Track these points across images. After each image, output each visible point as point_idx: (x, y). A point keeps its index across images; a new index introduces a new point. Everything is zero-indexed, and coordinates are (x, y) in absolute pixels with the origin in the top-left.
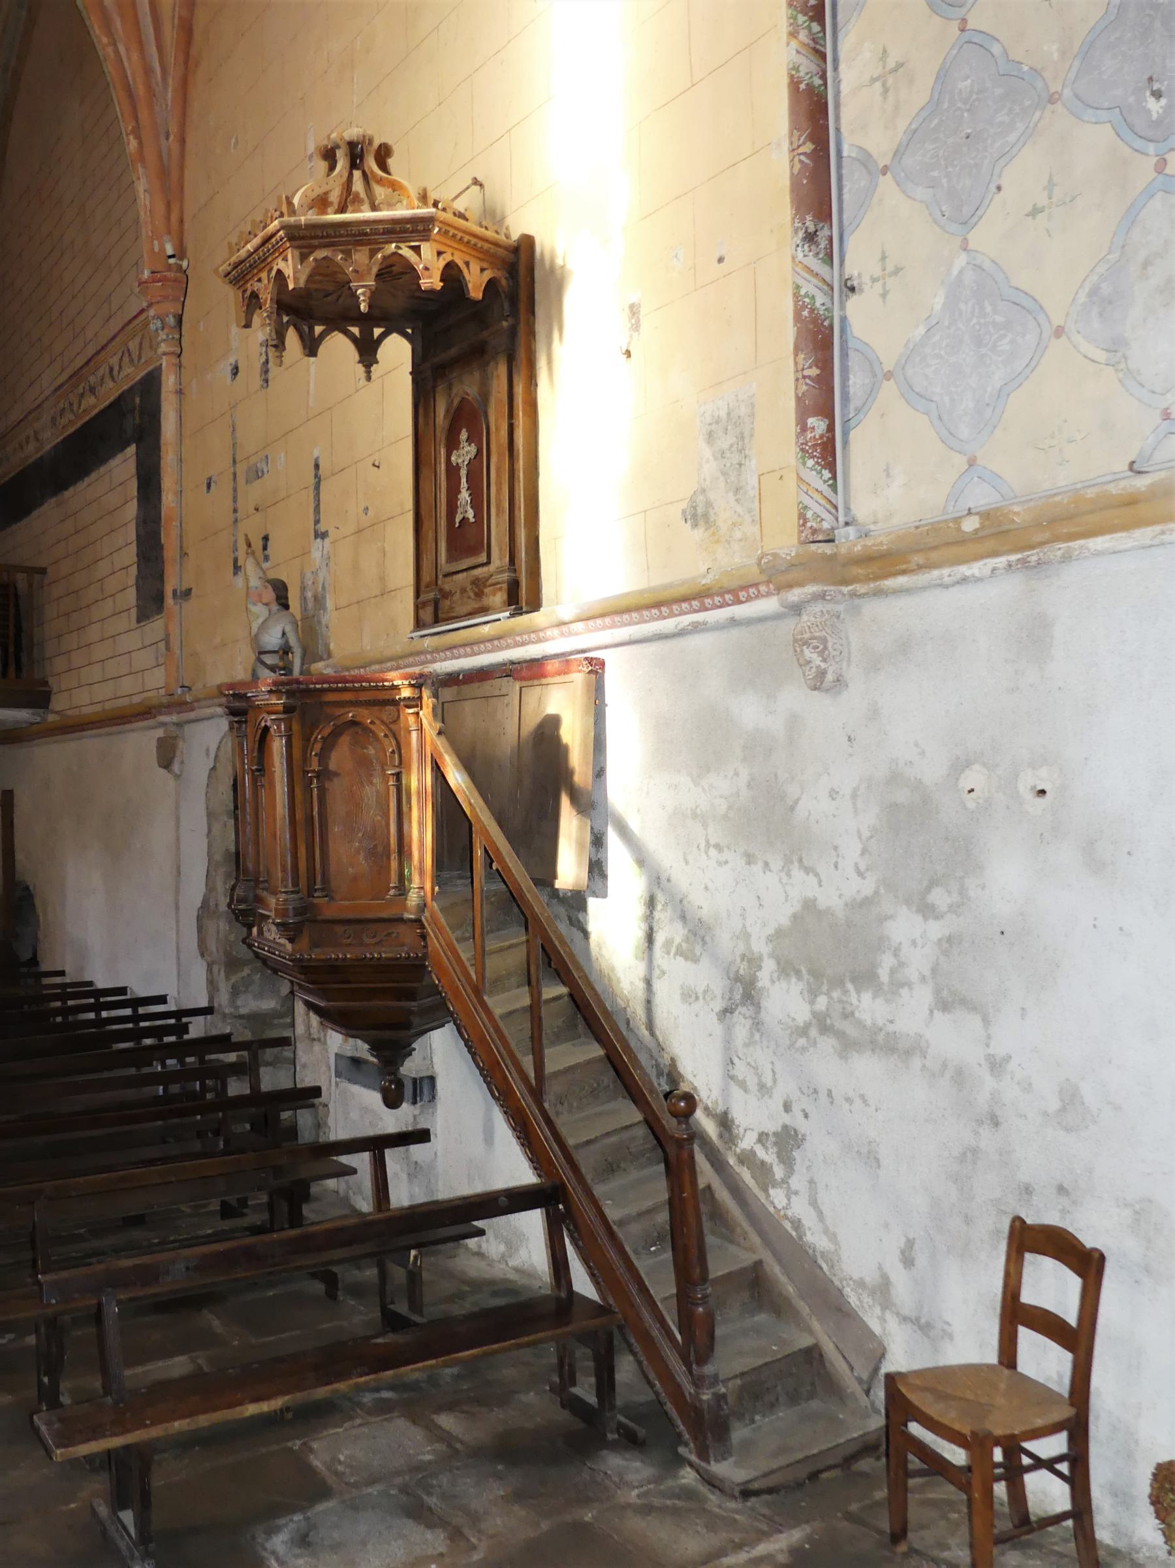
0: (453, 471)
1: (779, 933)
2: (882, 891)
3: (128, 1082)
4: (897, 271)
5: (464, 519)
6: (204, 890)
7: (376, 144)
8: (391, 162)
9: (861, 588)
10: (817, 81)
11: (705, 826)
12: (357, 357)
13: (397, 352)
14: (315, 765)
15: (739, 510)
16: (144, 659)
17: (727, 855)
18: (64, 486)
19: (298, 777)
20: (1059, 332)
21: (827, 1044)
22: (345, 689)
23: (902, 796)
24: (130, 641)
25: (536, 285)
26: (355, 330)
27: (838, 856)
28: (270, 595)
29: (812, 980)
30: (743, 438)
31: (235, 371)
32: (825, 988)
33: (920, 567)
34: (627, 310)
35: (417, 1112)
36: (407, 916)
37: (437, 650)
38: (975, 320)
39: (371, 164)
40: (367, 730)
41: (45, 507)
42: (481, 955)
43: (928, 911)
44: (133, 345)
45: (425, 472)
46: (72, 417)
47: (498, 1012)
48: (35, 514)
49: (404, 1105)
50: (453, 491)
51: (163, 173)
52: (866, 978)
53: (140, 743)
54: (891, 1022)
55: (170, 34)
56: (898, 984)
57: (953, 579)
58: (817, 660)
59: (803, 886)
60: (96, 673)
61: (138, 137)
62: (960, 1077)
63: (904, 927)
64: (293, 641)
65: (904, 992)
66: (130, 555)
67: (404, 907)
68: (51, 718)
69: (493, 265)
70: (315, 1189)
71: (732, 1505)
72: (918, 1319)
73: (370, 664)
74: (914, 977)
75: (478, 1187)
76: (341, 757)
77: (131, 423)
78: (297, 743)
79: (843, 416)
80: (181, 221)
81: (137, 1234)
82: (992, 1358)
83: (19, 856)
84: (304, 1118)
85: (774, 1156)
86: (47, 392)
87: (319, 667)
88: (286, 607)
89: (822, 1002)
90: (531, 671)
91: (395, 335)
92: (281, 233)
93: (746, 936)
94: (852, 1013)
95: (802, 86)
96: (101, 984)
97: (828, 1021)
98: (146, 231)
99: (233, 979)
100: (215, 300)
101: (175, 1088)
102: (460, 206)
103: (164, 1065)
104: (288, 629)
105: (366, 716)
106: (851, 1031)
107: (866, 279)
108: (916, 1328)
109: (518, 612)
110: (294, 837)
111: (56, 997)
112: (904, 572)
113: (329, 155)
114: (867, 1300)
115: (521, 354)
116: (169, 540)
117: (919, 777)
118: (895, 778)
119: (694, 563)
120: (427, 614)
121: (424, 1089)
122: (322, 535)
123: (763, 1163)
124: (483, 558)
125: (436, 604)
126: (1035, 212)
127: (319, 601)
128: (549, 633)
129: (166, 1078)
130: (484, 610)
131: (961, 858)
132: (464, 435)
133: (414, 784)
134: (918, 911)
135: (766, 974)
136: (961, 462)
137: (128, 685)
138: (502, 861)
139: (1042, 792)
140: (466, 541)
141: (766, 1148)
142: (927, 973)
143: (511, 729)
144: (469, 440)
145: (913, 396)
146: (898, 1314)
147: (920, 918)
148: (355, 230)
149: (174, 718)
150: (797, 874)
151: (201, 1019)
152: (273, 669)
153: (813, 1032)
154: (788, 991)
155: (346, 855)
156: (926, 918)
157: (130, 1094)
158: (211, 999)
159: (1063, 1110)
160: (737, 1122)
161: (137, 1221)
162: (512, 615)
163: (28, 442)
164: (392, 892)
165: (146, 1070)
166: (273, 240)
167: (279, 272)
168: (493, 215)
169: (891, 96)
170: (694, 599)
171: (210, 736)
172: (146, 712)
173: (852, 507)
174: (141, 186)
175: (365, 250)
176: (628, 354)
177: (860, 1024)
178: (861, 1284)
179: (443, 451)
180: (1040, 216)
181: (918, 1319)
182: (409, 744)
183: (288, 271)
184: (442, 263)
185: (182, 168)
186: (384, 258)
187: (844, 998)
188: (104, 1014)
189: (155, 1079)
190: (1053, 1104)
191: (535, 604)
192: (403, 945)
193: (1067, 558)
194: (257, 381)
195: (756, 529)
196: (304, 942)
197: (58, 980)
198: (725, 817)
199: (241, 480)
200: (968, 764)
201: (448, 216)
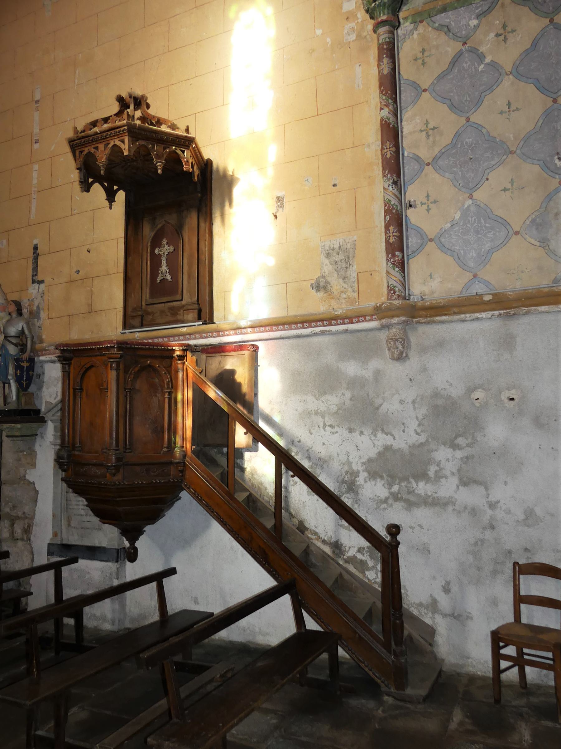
1: (370, 461)
2: (430, 440)
4: (435, 202)
5: (164, 280)
9: (422, 320)
10: (396, 126)
11: (323, 417)
12: (106, 198)
15: (346, 286)
17: (336, 429)
20: (517, 233)
21: (399, 505)
23: (440, 402)
27: (405, 427)
29: (389, 479)
30: (349, 257)
32: (397, 482)
33: (455, 313)
34: (275, 199)
35: (118, 566)
38: (476, 224)
40: (155, 370)
43: (455, 447)
52: (422, 476)
54: (436, 493)
56: (439, 476)
57: (471, 318)
58: (400, 347)
59: (382, 440)
62: (474, 512)
63: (442, 454)
65: (443, 480)
71: (420, 706)
72: (453, 614)
74: (448, 473)
79: (407, 253)
82: (512, 620)
85: (368, 557)
89: (395, 488)
90: (219, 350)
92: (126, 127)
93: (349, 463)
94: (413, 491)
95: (391, 126)
97: (399, 496)
106: (412, 498)
107: (418, 203)
108: (452, 618)
112: (446, 315)
114: (423, 611)
117: (449, 394)
118: (436, 395)
119: (317, 305)
123: (361, 560)
126: (505, 190)
128: (226, 333)
131: (473, 424)
134: (450, 447)
135: (360, 480)
136: (469, 276)
139: (512, 399)
141: (363, 555)
142: (455, 471)
145: (443, 248)
146: (441, 614)
147: (452, 450)
150: (380, 435)
153: (390, 501)
154: (375, 485)
156: (454, 450)
159: (527, 518)
160: (344, 545)
164: (165, 449)
166: (117, 130)
169: (431, 138)
170: (326, 321)
173: (411, 289)
176: (276, 217)
177: (418, 495)
178: (421, 605)
180: (507, 192)
181: (453, 614)
187: (408, 485)
190: (522, 517)
193: (528, 313)
195: (356, 294)
198: (336, 413)
200: (475, 389)
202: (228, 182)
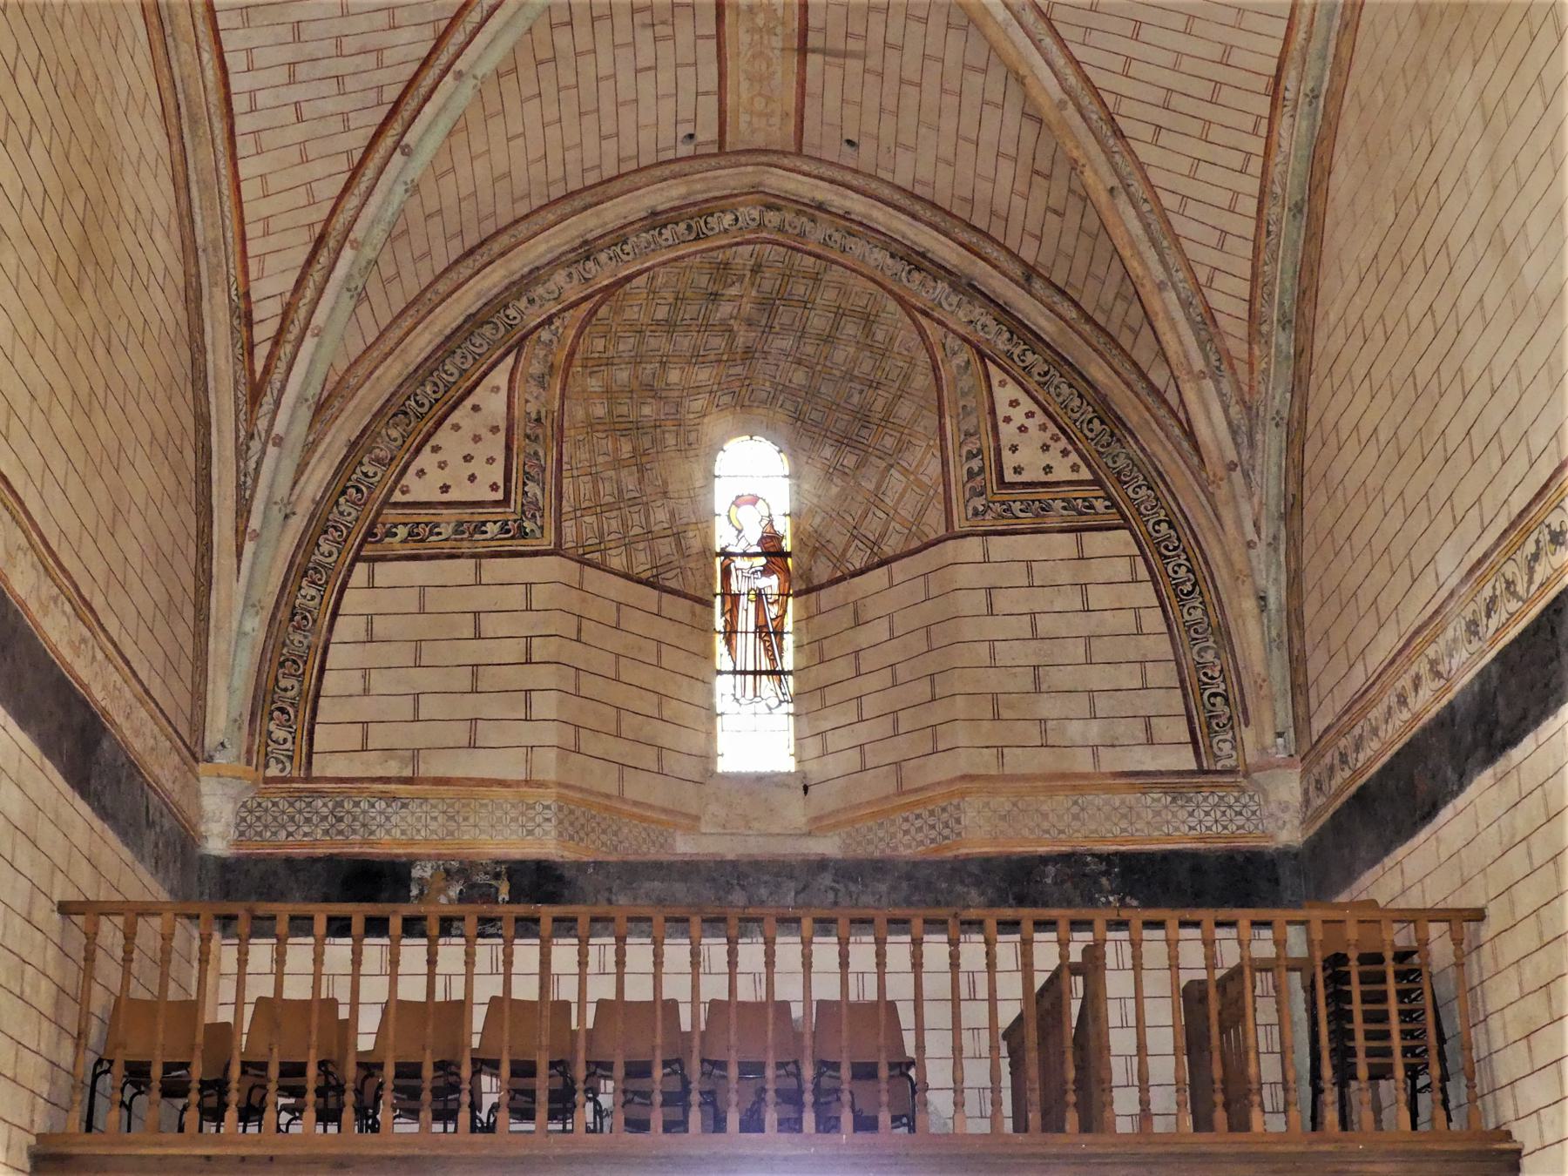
18: (1513, 740)
41: (1471, 791)
46: (1514, 605)
48: (1445, 813)
86: (1454, 581)
163: (1416, 687)
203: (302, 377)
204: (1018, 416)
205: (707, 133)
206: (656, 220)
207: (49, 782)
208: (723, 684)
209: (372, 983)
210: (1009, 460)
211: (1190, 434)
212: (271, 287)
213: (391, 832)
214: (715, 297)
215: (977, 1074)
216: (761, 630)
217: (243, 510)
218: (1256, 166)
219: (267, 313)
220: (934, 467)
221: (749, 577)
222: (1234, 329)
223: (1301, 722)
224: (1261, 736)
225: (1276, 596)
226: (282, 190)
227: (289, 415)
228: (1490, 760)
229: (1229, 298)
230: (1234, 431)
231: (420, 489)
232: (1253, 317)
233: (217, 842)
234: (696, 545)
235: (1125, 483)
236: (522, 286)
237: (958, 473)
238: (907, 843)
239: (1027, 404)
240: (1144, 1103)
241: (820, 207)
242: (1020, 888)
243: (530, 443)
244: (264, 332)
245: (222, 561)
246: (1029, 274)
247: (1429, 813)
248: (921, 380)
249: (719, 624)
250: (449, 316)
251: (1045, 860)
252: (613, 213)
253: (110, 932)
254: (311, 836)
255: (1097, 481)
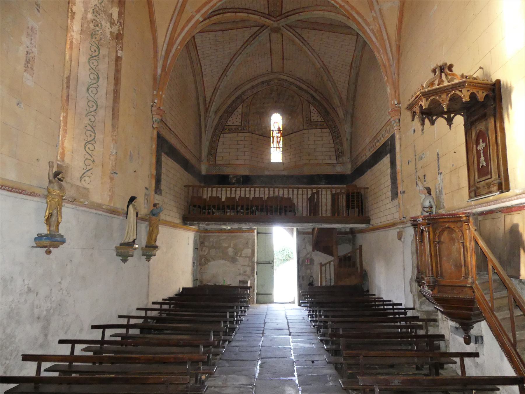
0: (478, 152)
3: (390, 327)
5: (483, 166)
6: (411, 274)
7: (274, 213)
8: (453, 69)
13: (459, 120)
14: (437, 240)
16: (394, 210)
18: (373, 166)
19: (432, 243)
22: (445, 218)
24: (389, 206)
25: (502, 94)
26: (446, 116)
28: (426, 191)
31: (414, 131)
36: (468, 285)
37: (476, 205)
39: (447, 71)
40: (453, 230)
42: (492, 299)
44: (388, 128)
45: (470, 153)
47: (499, 318)
49: (471, 344)
50: (479, 157)
51: (394, 84)
53: (393, 233)
55: (394, 48)
60: (382, 214)
61: (387, 76)
64: (433, 204)
66: (389, 183)
67: (467, 283)
68: (371, 226)
69: (486, 91)
70: (445, 366)
73: (456, 210)
75: (499, 374)
76: (445, 237)
77: (388, 148)
78: (431, 234)
80: (399, 95)
81: (391, 370)
83: (364, 263)
84: (442, 344)
87: (442, 211)
88: (431, 194)
91: (458, 116)
96: (385, 299)
98: (390, 99)
99: (420, 300)
100: (407, 115)
101: (404, 330)
102: (475, 76)
103: (400, 323)
104: (431, 200)
105: (452, 226)
109: (502, 192)
110: (431, 260)
111: (373, 301)
113: (434, 71)
115: (498, 115)
116: (399, 178)
120: (473, 194)
121: (479, 339)
122: (441, 174)
124: (489, 177)
125: (475, 191)
127: (440, 192)
129: (401, 327)
130: (491, 192)
132: (481, 141)
133: (468, 245)
137: (389, 217)
138: (497, 270)
140: (484, 172)
143: (502, 228)
144: (483, 142)
148: (441, 89)
149: (402, 226)
151: (412, 311)
152: (427, 212)
155: (448, 266)
157: (393, 330)
158: (414, 306)
161: (392, 366)
162: (500, 193)
165: (396, 324)
167: (421, 105)
168: (487, 75)
171: (410, 232)
172: (394, 225)
174: (388, 89)
175: (445, 94)
179: (475, 146)
182: (466, 234)
183: (423, 104)
184: (469, 93)
185: (398, 81)
186: (451, 95)
188: (386, 307)
189: (398, 327)
191: (508, 189)
192: (467, 294)
194: (420, 132)
196: (436, 291)
197: (374, 297)
199: (417, 160)
201: (471, 80)
202: (509, 91)
203: (213, 108)
204: (314, 112)
205: (270, 70)
206: (263, 83)
207: (183, 171)
208: (271, 149)
209: (224, 194)
210: (312, 118)
211: (338, 114)
212: (208, 95)
213: (228, 171)
214: (271, 94)
215: (305, 204)
216: (277, 141)
217: (206, 127)
218: (348, 77)
219: (208, 99)
220: (302, 120)
221: (276, 134)
222: (345, 101)
223: (351, 157)
224: (346, 158)
225: (349, 139)
226: (210, 80)
227: (211, 114)
228: (370, 168)
229: (344, 95)
230: (344, 115)
231: (230, 123)
232: (347, 99)
233: (204, 173)
234: (268, 129)
235: (329, 122)
236: (243, 93)
237: (305, 120)
238: (296, 172)
239: (315, 110)
240: (326, 208)
241: (286, 80)
242: (312, 180)
243: (245, 116)
244: (207, 102)
245: (203, 135)
246: (316, 91)
247: (364, 174)
248: (300, 107)
249: (272, 141)
250: (233, 98)
251: (315, 175)
252: (256, 82)
253: (191, 189)
254: (215, 172)
255: (324, 121)
